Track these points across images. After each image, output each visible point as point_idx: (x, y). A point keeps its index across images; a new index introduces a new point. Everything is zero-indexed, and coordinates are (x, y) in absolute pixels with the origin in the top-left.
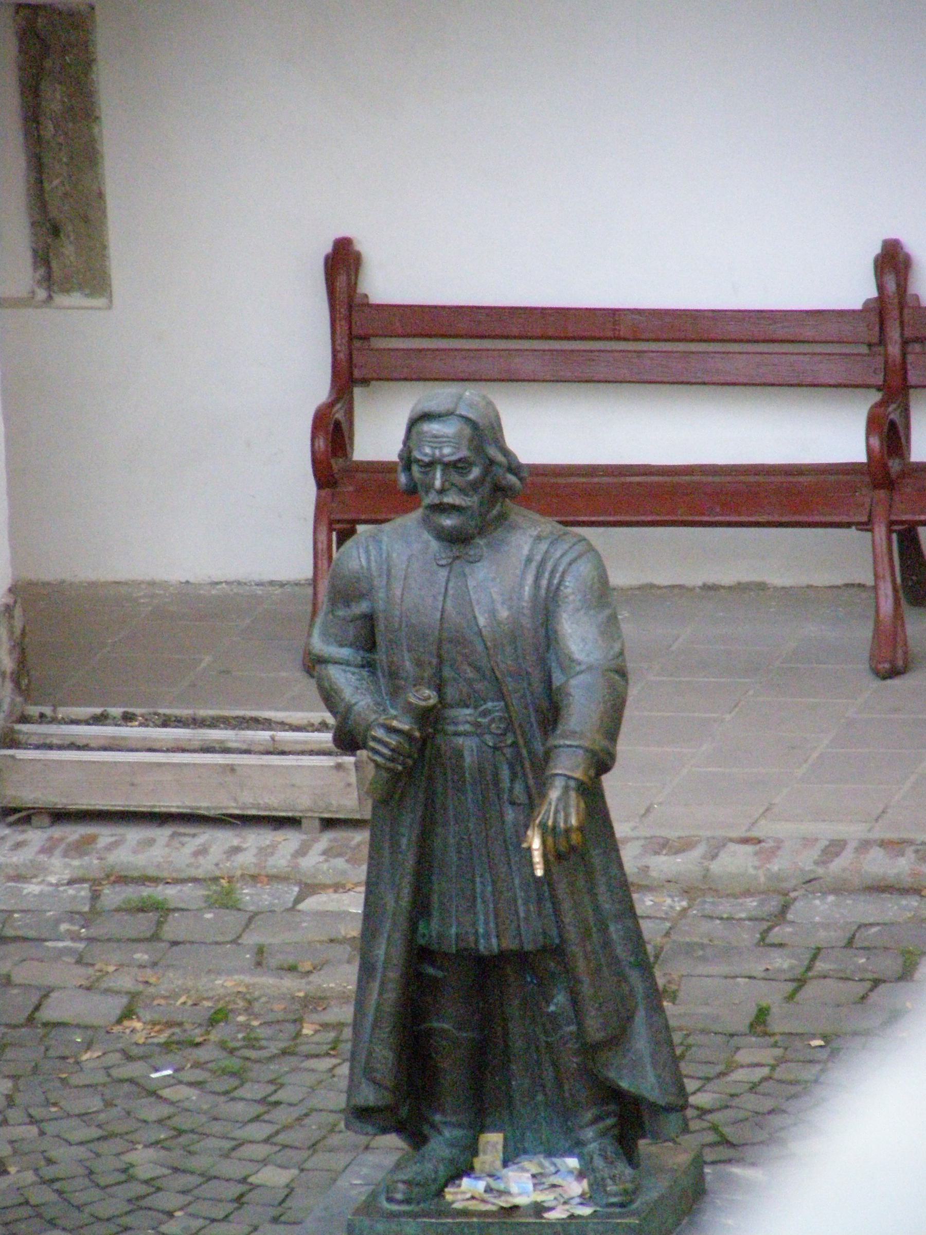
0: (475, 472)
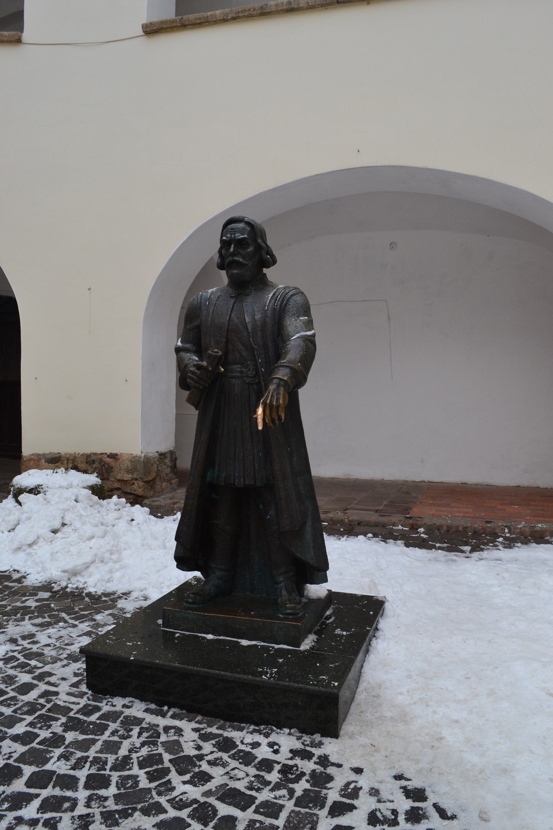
0: (251, 249)
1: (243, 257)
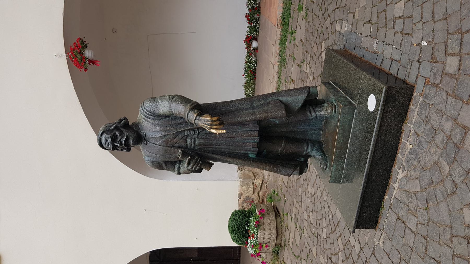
1: (122, 138)
